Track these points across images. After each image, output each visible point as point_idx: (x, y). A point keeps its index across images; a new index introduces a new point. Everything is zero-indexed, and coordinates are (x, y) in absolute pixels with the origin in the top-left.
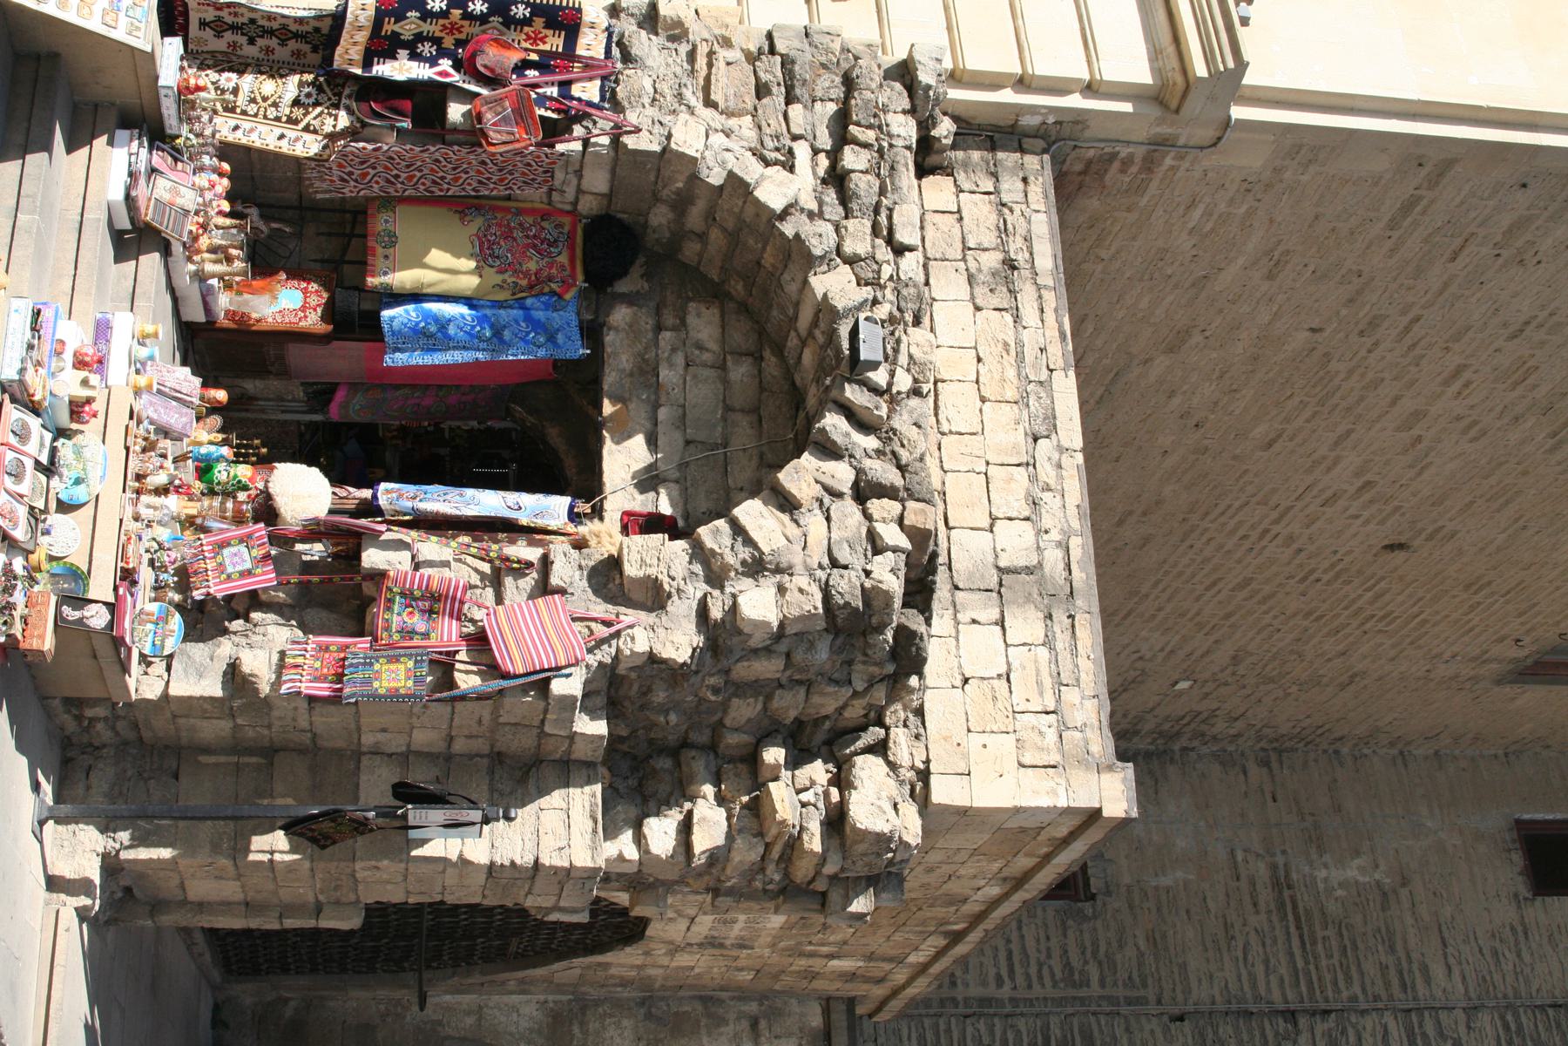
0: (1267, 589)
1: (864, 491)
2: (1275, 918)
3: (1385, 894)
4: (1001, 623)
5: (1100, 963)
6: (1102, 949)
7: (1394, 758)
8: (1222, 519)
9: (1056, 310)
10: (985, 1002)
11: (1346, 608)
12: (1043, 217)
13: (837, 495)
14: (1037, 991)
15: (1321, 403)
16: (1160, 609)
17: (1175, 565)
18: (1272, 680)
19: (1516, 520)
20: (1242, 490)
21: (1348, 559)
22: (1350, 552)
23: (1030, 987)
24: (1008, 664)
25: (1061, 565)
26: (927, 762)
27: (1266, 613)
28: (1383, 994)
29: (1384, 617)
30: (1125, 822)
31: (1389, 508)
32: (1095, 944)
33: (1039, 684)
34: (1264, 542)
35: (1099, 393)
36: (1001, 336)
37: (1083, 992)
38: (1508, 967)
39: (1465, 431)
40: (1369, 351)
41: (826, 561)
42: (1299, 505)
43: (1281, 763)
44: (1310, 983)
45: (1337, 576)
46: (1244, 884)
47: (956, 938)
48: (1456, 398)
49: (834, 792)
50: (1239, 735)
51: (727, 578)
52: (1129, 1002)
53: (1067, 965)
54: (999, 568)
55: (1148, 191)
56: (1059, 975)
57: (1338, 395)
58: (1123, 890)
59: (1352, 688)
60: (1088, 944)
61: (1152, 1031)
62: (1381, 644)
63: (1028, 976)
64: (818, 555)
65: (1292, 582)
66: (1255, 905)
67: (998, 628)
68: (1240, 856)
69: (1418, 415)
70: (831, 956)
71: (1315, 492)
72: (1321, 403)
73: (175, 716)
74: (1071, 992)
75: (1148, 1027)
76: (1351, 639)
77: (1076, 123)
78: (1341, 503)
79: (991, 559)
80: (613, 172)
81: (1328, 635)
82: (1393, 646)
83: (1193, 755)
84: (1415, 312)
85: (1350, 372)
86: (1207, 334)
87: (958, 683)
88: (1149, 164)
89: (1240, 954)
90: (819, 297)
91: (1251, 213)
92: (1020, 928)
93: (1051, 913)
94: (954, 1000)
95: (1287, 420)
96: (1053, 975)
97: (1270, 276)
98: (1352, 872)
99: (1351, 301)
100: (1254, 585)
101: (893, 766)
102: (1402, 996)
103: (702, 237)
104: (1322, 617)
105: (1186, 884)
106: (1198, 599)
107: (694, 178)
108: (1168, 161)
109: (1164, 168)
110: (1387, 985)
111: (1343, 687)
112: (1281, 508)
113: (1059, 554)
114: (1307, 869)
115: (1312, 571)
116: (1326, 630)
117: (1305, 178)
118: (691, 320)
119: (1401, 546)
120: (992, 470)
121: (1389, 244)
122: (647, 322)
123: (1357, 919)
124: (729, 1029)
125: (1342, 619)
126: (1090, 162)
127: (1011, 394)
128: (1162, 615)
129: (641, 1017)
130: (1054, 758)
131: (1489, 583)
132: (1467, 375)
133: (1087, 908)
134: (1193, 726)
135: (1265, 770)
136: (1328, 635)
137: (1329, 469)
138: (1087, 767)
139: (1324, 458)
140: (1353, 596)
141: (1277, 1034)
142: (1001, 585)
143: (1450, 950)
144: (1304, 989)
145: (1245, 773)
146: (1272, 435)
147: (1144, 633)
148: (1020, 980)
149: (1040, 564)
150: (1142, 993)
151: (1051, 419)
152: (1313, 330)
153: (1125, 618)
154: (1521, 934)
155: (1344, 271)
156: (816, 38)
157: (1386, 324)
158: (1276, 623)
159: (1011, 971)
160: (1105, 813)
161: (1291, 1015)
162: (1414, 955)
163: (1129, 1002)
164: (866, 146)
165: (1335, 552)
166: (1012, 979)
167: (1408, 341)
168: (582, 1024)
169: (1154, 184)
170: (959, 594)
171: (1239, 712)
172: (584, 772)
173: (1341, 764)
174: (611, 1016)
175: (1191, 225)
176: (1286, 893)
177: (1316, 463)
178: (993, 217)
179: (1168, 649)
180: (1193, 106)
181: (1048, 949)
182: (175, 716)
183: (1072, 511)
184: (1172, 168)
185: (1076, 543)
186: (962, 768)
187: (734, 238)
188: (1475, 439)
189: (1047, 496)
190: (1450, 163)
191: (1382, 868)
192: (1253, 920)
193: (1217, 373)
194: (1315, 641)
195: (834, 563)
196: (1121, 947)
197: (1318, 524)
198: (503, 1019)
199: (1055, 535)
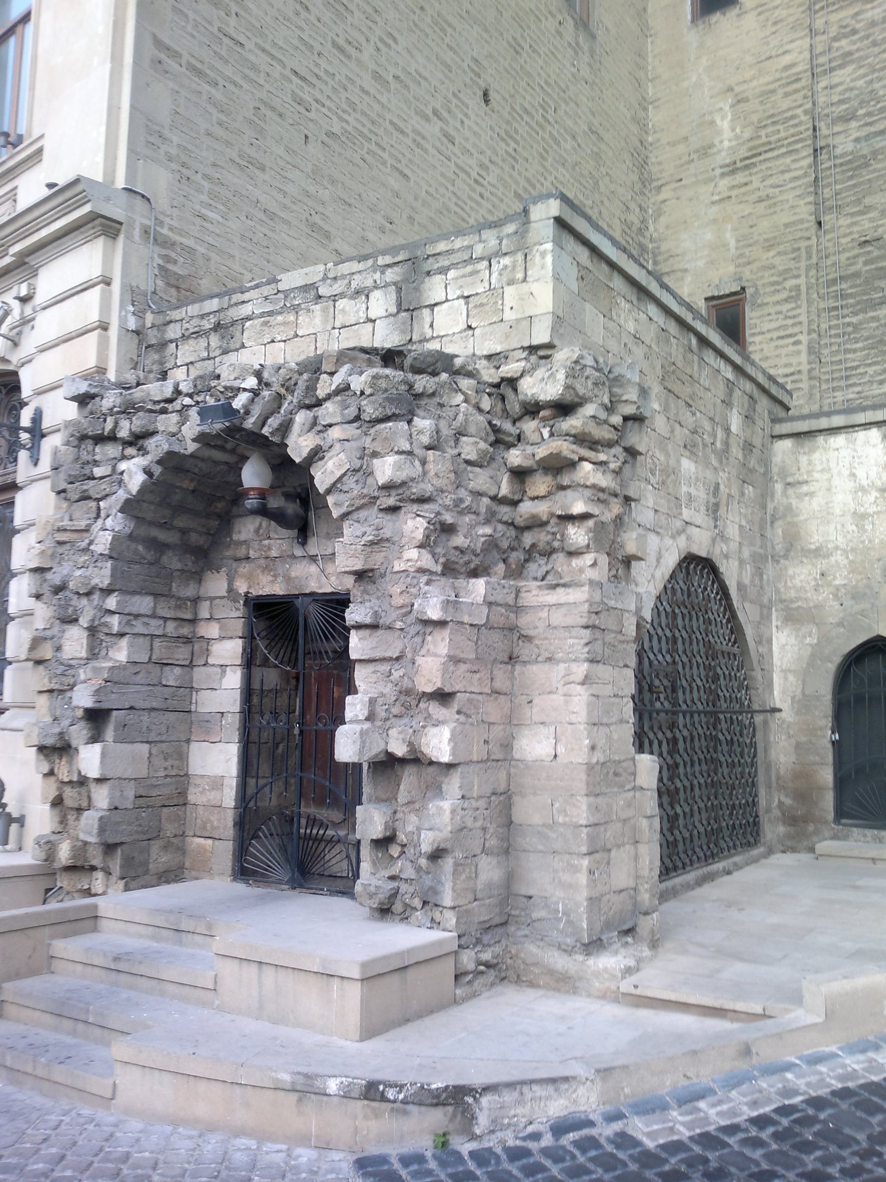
0: (523, 183)
2: (755, 170)
3: (739, 101)
5: (785, 279)
6: (775, 279)
7: (655, 108)
8: (467, 208)
10: (811, 350)
12: (189, 308)
13: (315, 422)
14: (803, 318)
18: (597, 183)
19: (461, 17)
20: (443, 196)
21: (497, 129)
22: (492, 128)
23: (800, 323)
24: (458, 298)
25: (396, 269)
28: (802, 93)
29: (544, 109)
31: (454, 101)
32: (772, 284)
33: (471, 274)
34: (485, 183)
36: (258, 328)
37: (803, 289)
38: (784, 13)
39: (388, 46)
40: (324, 106)
43: (658, 179)
45: (511, 137)
46: (734, 193)
48: (361, 51)
49: (542, 414)
52: (809, 257)
53: (786, 300)
54: (398, 312)
56: (793, 305)
57: (361, 128)
58: (738, 270)
59: (601, 132)
60: (773, 288)
62: (565, 111)
63: (794, 325)
64: (351, 430)
66: (746, 184)
67: (436, 309)
68: (716, 198)
69: (376, 76)
70: (728, 430)
71: (443, 148)
74: (804, 296)
76: (562, 131)
77: (132, 291)
79: (392, 319)
80: (134, 593)
82: (567, 104)
83: (655, 235)
84: (288, 72)
87: (471, 332)
89: (777, 190)
92: (763, 333)
93: (754, 314)
94: (809, 371)
95: (384, 163)
96: (793, 309)
97: (263, 169)
98: (724, 124)
99: (280, 115)
102: (804, 80)
103: (184, 532)
104: (545, 149)
105: (734, 230)
107: (131, 537)
108: (165, 231)
109: (170, 234)
110: (797, 91)
112: (457, 171)
113: (389, 271)
114: (723, 154)
115: (507, 152)
116: (555, 147)
117: (176, 140)
118: (243, 537)
119: (486, 94)
120: (338, 324)
121: (231, 87)
122: (244, 568)
123: (755, 118)
124: (794, 502)
125: (547, 136)
126: (168, 284)
129: (787, 562)
130: (520, 257)
131: (514, 39)
132: (341, 41)
134: (633, 235)
135: (663, 189)
138: (527, 231)
141: (829, 159)
142: (408, 310)
143: (773, 53)
144: (799, 146)
145: (665, 201)
146: (397, 174)
148: (796, 330)
149: (395, 284)
150: (803, 250)
151: (305, 288)
154: (764, 8)
155: (256, 119)
159: (790, 336)
160: (557, 214)
162: (777, 76)
163: (809, 257)
164: (116, 423)
166: (796, 335)
167: (313, 80)
168: (792, 601)
170: (414, 338)
172: (523, 595)
173: (658, 140)
174: (786, 582)
175: (220, 219)
176: (739, 165)
177: (418, 145)
181: (777, 313)
184: (171, 229)
186: (526, 323)
187: (180, 509)
188: (395, 40)
189: (354, 285)
190: (158, 43)
191: (721, 105)
192: (756, 184)
193: (347, 207)
194: (563, 153)
195: (357, 418)
196: (774, 267)
198: (789, 655)
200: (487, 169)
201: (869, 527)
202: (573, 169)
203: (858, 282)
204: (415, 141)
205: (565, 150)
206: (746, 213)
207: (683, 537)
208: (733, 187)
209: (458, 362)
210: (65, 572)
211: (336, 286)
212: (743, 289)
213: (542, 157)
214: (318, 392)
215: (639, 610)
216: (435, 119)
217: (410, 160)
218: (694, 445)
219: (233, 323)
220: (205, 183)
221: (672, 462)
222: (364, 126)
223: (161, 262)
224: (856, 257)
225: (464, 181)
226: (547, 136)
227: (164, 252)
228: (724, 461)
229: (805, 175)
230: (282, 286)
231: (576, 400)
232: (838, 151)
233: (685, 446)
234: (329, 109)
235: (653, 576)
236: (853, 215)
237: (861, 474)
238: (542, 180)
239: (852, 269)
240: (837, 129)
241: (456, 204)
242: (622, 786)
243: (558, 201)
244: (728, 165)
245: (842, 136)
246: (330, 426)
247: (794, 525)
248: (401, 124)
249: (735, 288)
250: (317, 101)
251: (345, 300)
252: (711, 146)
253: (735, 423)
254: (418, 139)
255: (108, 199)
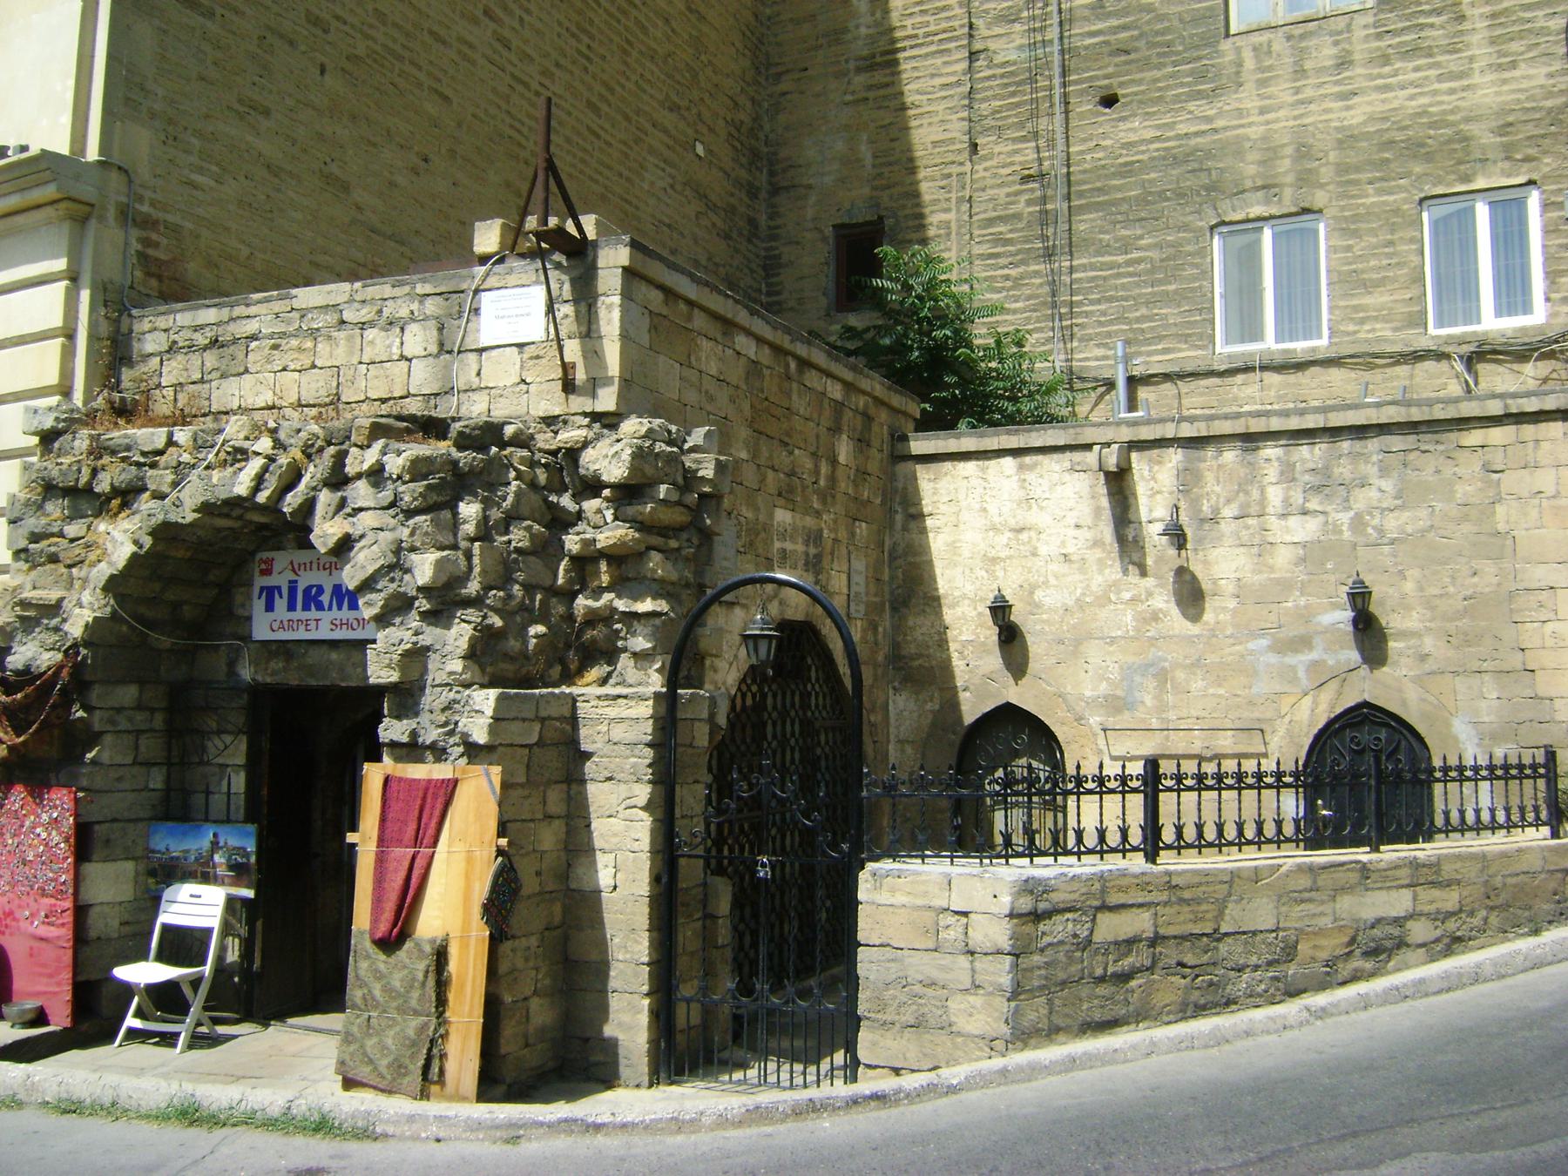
1: (338, 480)
4: (481, 351)
8: (525, 130)
9: (247, 305)
11: (619, 21)
12: (178, 316)
13: (343, 503)
15: (401, 58)
16: (621, 175)
17: (574, 166)
20: (494, 117)
21: (566, 23)
22: (560, 24)
26: (585, 414)
27: (623, 87)
30: (634, 245)
35: (393, 244)
36: (267, 351)
41: (392, 512)
42: (510, 68)
44: (950, 40)
45: (585, 31)
46: (871, 95)
47: (805, 364)
50: (753, 100)
51: (405, 594)
55: (149, 227)
57: (391, 45)
61: (985, 170)
64: (386, 518)
65: (591, 68)
68: (849, 98)
70: (834, 462)
71: (496, 57)
72: (401, 58)
73: (527, 1045)
75: (981, 174)
77: (105, 289)
78: (506, 33)
81: (646, 33)
83: (771, 136)
85: (367, 37)
86: (328, 160)
87: (524, 387)
88: (146, 223)
90: (197, 515)
91: (199, 134)
95: (420, 85)
97: (267, 113)
99: (291, 43)
100: (594, 100)
101: (586, 444)
103: (176, 606)
106: (609, 144)
109: (151, 211)
111: (702, 18)
113: (429, 302)
114: (860, 43)
115: (579, 52)
116: (642, 37)
117: (160, 92)
120: (366, 359)
125: (630, 24)
126: (149, 274)
127: (309, 344)
128: (626, 173)
133: (889, 222)
136: (646, 33)
137: (471, 46)
139: (459, 52)
140: (605, 16)
141: (988, 67)
144: (952, 45)
145: (785, 94)
147: (646, 187)
152: (323, 72)
153: (630, 203)
156: (16, 514)
157: (317, 12)
158: (634, 78)
160: (627, 263)
161: (973, 56)
165: (559, 35)
169: (170, 218)
171: (729, 102)
173: (778, 14)
175: (212, 183)
176: (878, 59)
177: (465, 57)
178: (180, 357)
179: (662, 165)
180: (87, 192)
182: (527, 1045)
183: (398, 292)
184: (152, 204)
185: (420, 289)
195: (392, 505)
197: (529, 51)
199: (415, 306)
200: (551, 76)
201: (1000, 574)
202: (665, 62)
203: (1020, 226)
204: (459, 52)
205: (655, 39)
206: (887, 122)
207: (775, 603)
208: (870, 88)
209: (509, 430)
210: (30, 654)
211: (364, 311)
212: (881, 218)
213: (625, 52)
214: (347, 469)
215: (712, 716)
216: (487, 20)
217: (452, 78)
218: (791, 490)
219: (235, 341)
220: (194, 141)
221: (762, 518)
222: (395, 40)
223: (139, 247)
224: (1017, 193)
225: (522, 95)
226: (630, 24)
227: (144, 234)
228: (829, 499)
229: (958, 83)
230: (296, 304)
231: (644, 481)
232: (998, 59)
233: (780, 495)
234: (353, 26)
235: (736, 656)
236: (1014, 140)
237: (992, 508)
238: (623, 81)
239: (1013, 209)
240: (997, 30)
241: (512, 126)
242: (690, 916)
243: (628, 249)
244: (864, 59)
245: (1004, 39)
246: (361, 510)
247: (916, 566)
248: (443, 32)
249: (870, 217)
250: (337, 18)
251: (375, 331)
252: (846, 30)
253: (844, 451)
254: (465, 49)
255: (77, 178)
